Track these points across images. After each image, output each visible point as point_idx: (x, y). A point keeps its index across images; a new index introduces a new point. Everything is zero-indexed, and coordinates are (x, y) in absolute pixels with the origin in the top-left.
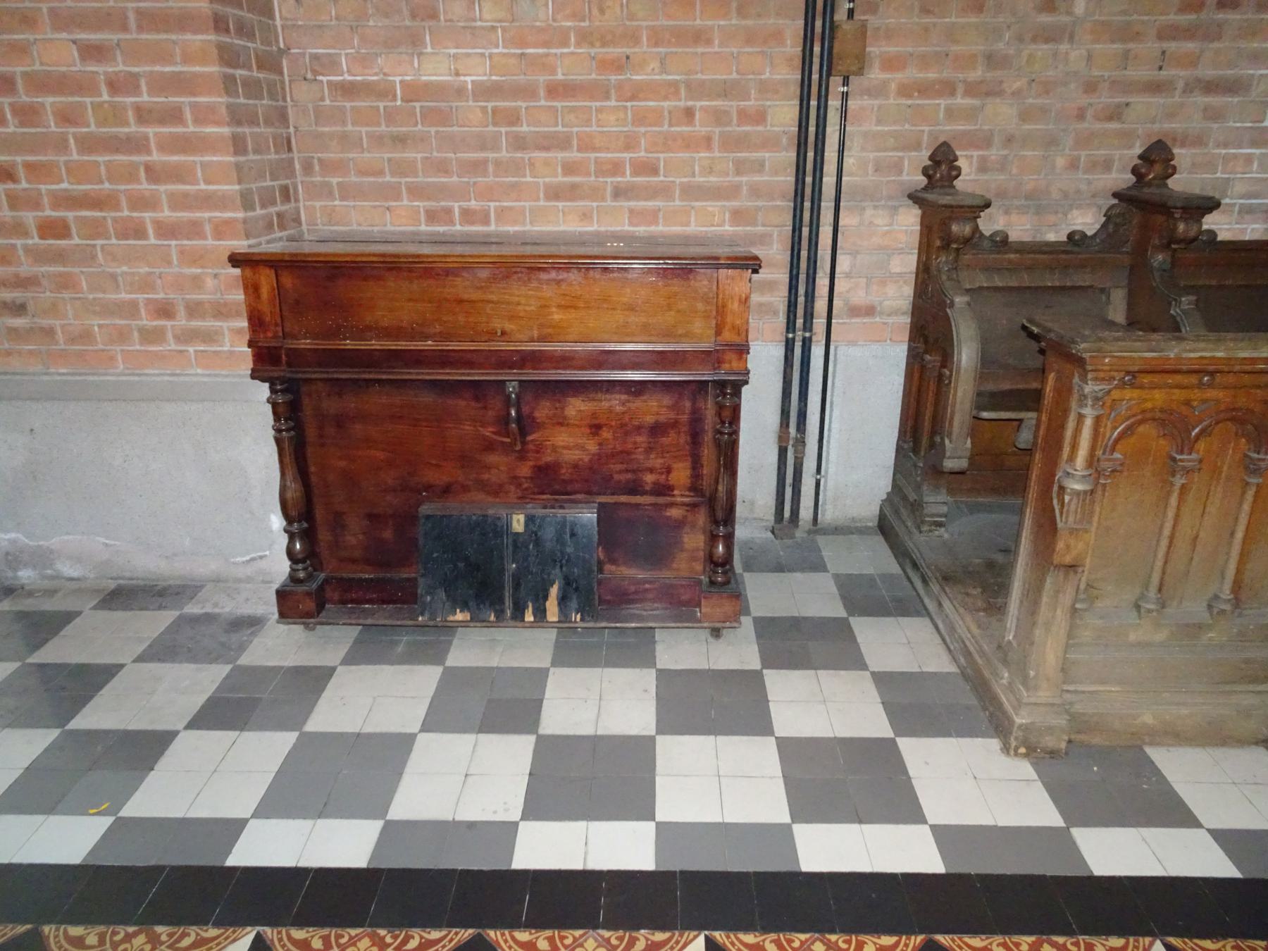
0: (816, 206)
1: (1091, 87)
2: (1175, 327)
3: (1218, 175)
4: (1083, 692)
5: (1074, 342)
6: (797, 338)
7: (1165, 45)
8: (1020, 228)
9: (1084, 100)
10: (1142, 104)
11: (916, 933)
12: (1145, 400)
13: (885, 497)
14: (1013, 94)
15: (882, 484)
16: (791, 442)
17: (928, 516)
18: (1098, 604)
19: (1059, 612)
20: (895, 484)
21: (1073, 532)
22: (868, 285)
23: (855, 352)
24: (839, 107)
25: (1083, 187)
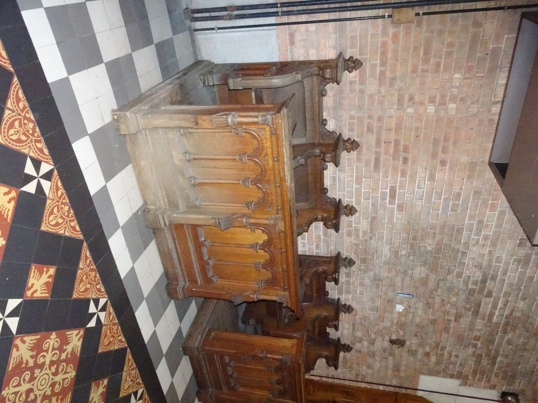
0: (337, 10)
1: (380, 119)
2: (295, 158)
3: (347, 168)
4: (147, 138)
5: (286, 108)
6: (278, 9)
7: (393, 143)
8: (328, 101)
9: (375, 118)
10: (372, 138)
11: (83, 236)
12: (266, 140)
13: (212, 61)
14: (380, 90)
15: (218, 60)
16: (230, 13)
17: (207, 78)
18: (184, 139)
19: (177, 122)
20: (218, 65)
21: (211, 121)
22: (303, 40)
23: (274, 39)
24: (379, 15)
25: (343, 123)
